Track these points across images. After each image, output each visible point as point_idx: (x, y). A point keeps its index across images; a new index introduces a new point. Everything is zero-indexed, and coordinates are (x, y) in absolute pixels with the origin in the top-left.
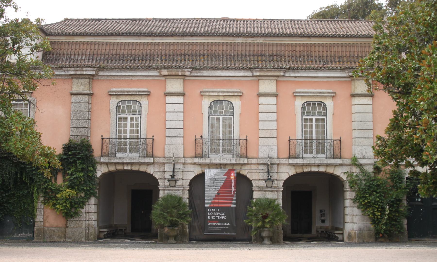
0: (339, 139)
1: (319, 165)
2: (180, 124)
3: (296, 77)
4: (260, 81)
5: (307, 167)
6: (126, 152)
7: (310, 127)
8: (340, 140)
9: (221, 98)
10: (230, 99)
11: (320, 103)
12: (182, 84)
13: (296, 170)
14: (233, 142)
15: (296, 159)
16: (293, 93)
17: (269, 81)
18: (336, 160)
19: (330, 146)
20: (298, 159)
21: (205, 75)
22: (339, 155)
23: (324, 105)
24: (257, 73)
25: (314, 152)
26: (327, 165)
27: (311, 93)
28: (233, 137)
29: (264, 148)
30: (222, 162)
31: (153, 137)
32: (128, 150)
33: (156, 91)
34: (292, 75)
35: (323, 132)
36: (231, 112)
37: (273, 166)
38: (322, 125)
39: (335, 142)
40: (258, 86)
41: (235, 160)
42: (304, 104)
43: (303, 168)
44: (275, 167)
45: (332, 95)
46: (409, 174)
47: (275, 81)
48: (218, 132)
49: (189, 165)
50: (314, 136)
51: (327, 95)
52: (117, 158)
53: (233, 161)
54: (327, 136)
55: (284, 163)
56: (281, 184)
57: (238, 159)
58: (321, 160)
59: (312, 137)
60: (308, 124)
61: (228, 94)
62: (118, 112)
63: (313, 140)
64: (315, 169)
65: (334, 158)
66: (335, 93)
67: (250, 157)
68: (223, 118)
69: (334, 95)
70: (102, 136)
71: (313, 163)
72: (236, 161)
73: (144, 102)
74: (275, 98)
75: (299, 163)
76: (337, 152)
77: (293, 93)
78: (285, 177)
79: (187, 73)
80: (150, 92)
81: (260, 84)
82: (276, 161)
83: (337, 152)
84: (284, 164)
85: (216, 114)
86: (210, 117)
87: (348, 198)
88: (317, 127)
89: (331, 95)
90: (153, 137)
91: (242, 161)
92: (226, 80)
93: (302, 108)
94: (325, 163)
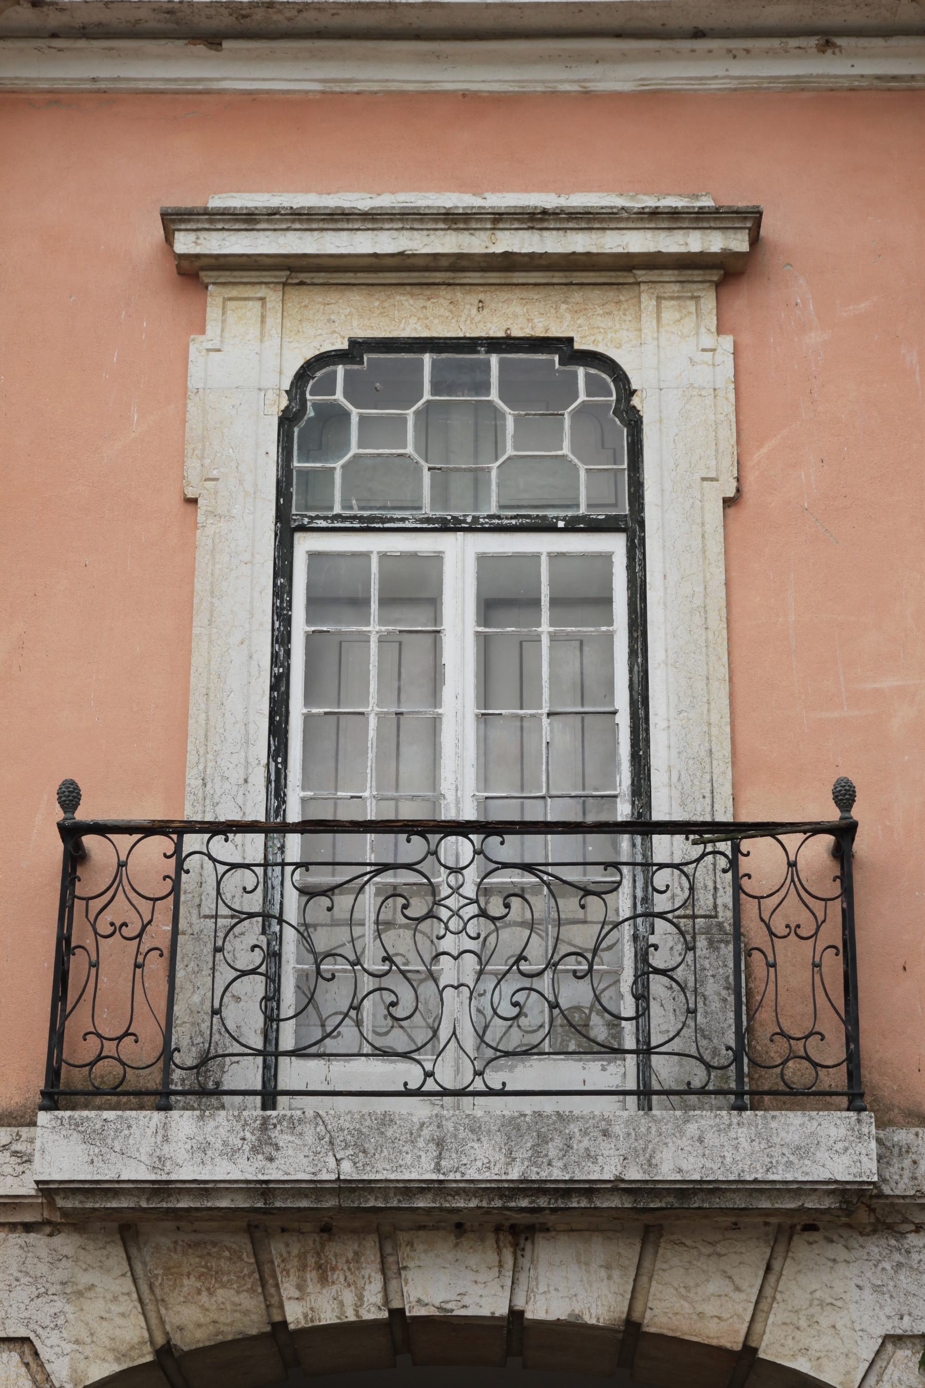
0: (833, 814)
1: (518, 1219)
5: (340, 1251)
13: (148, 1301)
16: (173, 220)
18: (792, 1124)
20: (183, 1122)
22: (833, 1050)
23: (593, 387)
39: (762, 854)
43: (265, 1281)
45: (714, 242)
51: (637, 242)
52: (713, 1295)
58: (541, 1132)
61: (386, 242)
64: (454, 1286)
66: (751, 220)
68: (483, 559)
69: (739, 243)
71: (419, 1167)
73: (671, 353)
75: (187, 1172)
76: (796, 984)
77: (173, 220)
83: (796, 984)
86: (304, 544)
89: (694, 242)
93: (287, 420)
94: (607, 1168)
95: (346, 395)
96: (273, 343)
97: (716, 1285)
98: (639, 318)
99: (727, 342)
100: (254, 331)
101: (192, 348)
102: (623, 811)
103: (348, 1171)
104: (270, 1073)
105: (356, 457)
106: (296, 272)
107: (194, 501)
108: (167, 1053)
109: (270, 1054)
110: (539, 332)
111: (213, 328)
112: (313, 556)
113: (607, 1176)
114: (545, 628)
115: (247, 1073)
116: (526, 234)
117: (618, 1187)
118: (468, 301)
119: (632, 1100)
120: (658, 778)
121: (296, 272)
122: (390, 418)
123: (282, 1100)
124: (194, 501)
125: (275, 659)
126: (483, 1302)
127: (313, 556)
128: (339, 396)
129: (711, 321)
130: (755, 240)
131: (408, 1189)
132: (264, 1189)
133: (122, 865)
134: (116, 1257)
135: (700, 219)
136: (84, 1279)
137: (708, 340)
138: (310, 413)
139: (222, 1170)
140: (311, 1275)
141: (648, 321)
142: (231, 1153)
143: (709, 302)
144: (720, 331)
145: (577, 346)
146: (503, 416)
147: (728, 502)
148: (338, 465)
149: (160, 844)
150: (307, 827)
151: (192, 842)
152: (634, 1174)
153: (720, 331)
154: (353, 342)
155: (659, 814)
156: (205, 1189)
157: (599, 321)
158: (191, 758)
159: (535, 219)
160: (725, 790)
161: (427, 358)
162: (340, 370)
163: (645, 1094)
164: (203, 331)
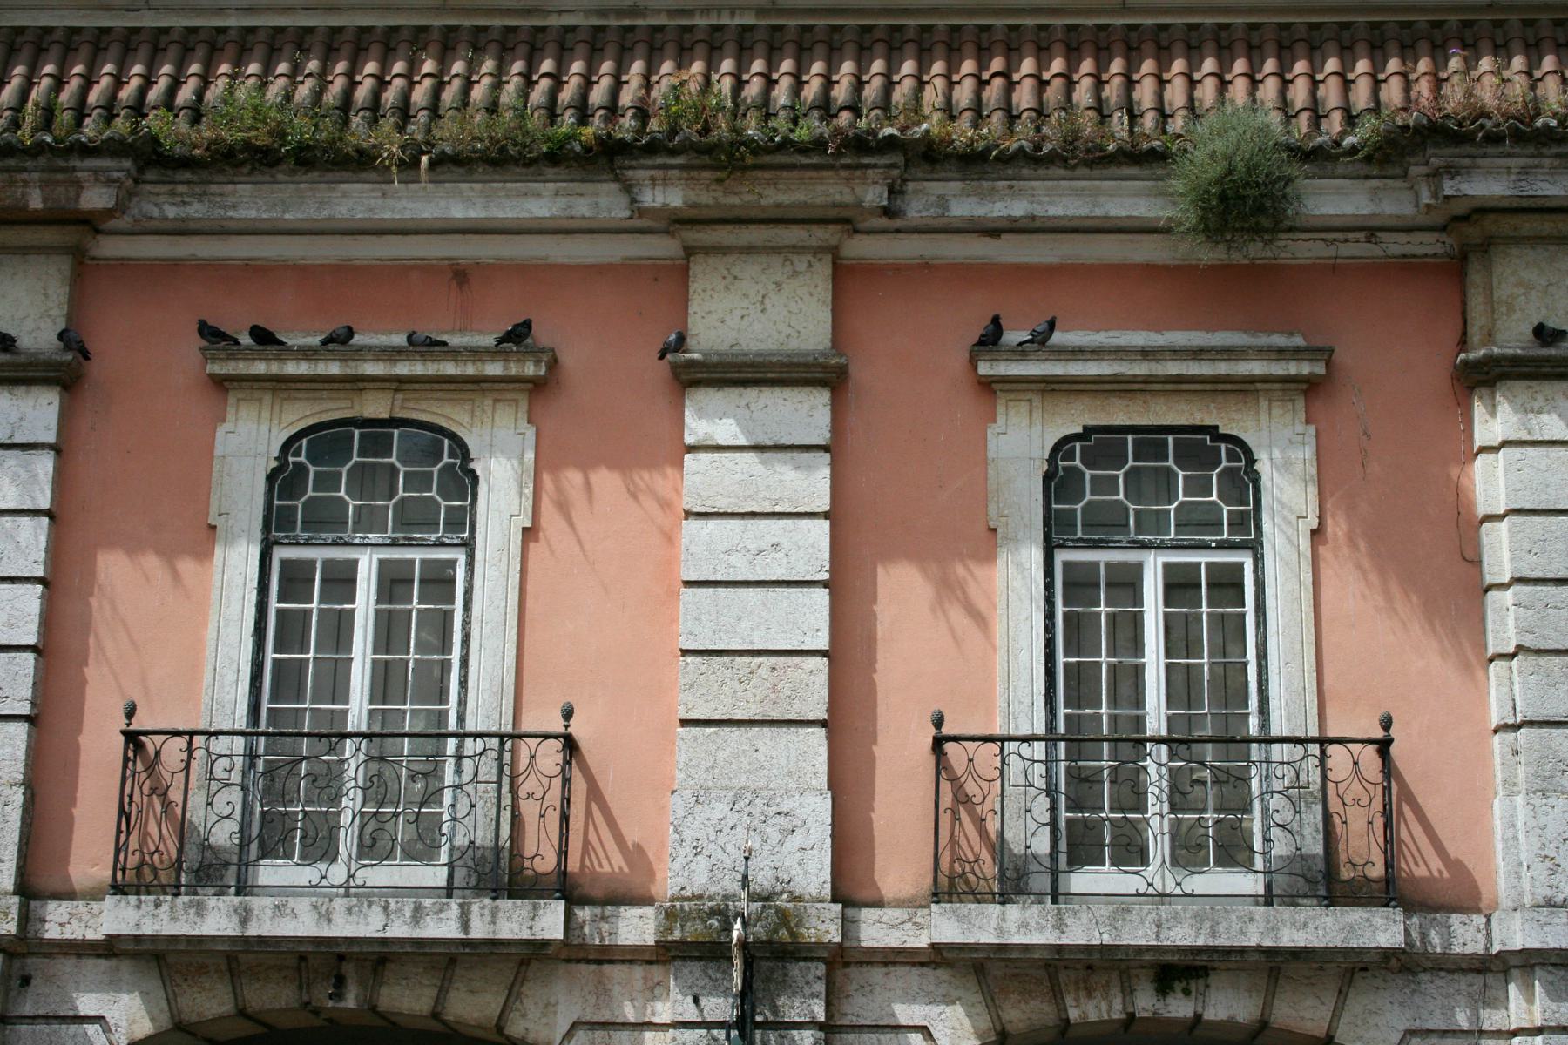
0: (1379, 734)
3: (993, 231)
4: (698, 267)
6: (330, 855)
7: (1124, 634)
8: (1384, 746)
9: (376, 407)
10: (448, 410)
11: (1201, 446)
12: (824, 290)
14: (459, 757)
15: (994, 910)
17: (777, 260)
19: (1296, 794)
20: (1013, 911)
21: (248, 212)
23: (1232, 456)
24: (668, 196)
25: (1159, 847)
27: (1119, 353)
28: (461, 719)
29: (720, 809)
30: (344, 926)
32: (347, 842)
33: (591, 345)
34: (964, 208)
35: (1231, 688)
36: (1239, 522)
38: (1218, 621)
40: (685, 302)
42: (1062, 448)
45: (1305, 369)
47: (824, 269)
48: (1125, 689)
50: (1156, 714)
51: (1256, 368)
53: (443, 926)
54: (1264, 710)
55: (893, 940)
57: (480, 907)
59: (1139, 722)
60: (1103, 609)
62: (275, 528)
63: (1142, 742)
65: (1330, 900)
67: (597, 892)
68: (1166, 566)
69: (1320, 369)
72: (465, 925)
74: (822, 398)
79: (96, 198)
80: (554, 364)
81: (696, 286)
82: (824, 926)
85: (329, 537)
86: (1061, 557)
88: (1179, 637)
89: (1293, 368)
91: (512, 921)
92: (426, 269)
93: (1048, 478)
95: (1082, 461)
96: (1037, 428)
98: (1258, 413)
99: (1312, 430)
100: (1025, 422)
101: (989, 432)
105: (1090, 502)
106: (1050, 387)
107: (994, 530)
110: (1198, 423)
111: (1001, 420)
112: (1066, 564)
113: (1252, 944)
114: (1204, 609)
115: (1041, 882)
116: (1191, 363)
117: (1259, 949)
120: (1274, 704)
121: (1050, 387)
122: (1110, 477)
124: (994, 530)
126: (806, 639)
127: (1066, 564)
128: (1078, 462)
129: (1303, 416)
130: (1328, 364)
131: (1140, 950)
132: (1059, 949)
135: (1296, 353)
137: (1300, 428)
138: (1061, 473)
141: (1264, 417)
142: (1041, 929)
143: (1300, 403)
144: (1307, 422)
145: (1221, 431)
146: (1176, 475)
147: (1313, 532)
148: (1079, 506)
149: (181, 742)
151: (1011, 746)
152: (1268, 943)
153: (1307, 422)
154: (1085, 428)
155: (1275, 731)
156: (1026, 948)
157: (1234, 415)
159: (1198, 353)
161: (1130, 438)
162: (1078, 445)
164: (994, 421)
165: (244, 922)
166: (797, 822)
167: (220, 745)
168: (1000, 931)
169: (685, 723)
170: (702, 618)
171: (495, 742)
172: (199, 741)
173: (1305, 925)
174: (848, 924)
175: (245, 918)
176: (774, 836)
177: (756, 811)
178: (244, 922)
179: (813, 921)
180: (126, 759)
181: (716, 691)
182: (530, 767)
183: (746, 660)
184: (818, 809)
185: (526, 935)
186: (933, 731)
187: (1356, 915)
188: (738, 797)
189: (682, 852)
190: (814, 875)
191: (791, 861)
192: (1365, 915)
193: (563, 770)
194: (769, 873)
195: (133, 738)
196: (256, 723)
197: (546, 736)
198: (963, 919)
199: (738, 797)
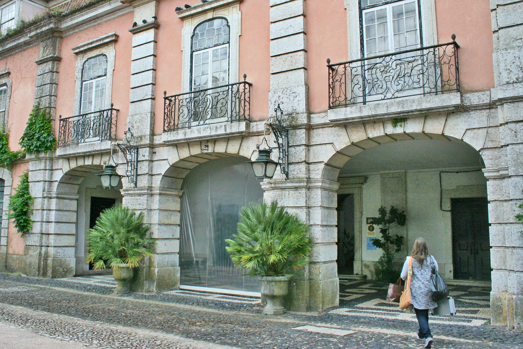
0: (452, 41)
1: (399, 119)
2: (299, 42)
5: (376, 126)
15: (343, 109)
20: (348, 109)
26: (426, 114)
31: (454, 37)
37: (298, 131)
41: (43, 163)
44: (301, 135)
46: (274, 205)
49: (161, 149)
55: (322, 121)
56: (317, 172)
70: (329, 61)
72: (226, 130)
76: (449, 73)
78: (325, 154)
84: (323, 126)
87: (319, 241)
90: (454, 37)
97: (437, 124)
102: (419, 47)
103: (373, 113)
104: (364, 99)
108: (346, 98)
109: (364, 96)
115: (361, 100)
117: (416, 110)
118: (83, 35)
119: (422, 95)
120: (424, 40)
123: (367, 103)
125: (360, 32)
133: (444, 51)
134: (344, 130)
136: (340, 133)
139: (354, 115)
140: (373, 129)
149: (343, 66)
150: (367, 59)
151: (347, 65)
152: (418, 108)
155: (424, 46)
156: (353, 119)
158: (349, 51)
160: (436, 40)
163: (424, 94)
165: (185, 135)
166: (297, 94)
167: (354, 65)
168: (345, 114)
169: (273, 74)
170: (276, 48)
171: (432, 49)
172: (177, 97)
173: (430, 101)
174: (309, 118)
175: (185, 134)
176: (292, 98)
177: (288, 93)
178: (185, 135)
179: (300, 119)
180: (329, 73)
181: (277, 65)
182: (444, 54)
183: (285, 55)
184: (302, 90)
185: (237, 131)
186: (327, 64)
187: (445, 96)
188: (284, 90)
189: (271, 106)
190: (301, 107)
191: (296, 104)
192: (448, 96)
193: (455, 54)
194: (291, 108)
195: (330, 67)
196: (191, 90)
197: (448, 44)
198: (336, 113)
199: (284, 90)
